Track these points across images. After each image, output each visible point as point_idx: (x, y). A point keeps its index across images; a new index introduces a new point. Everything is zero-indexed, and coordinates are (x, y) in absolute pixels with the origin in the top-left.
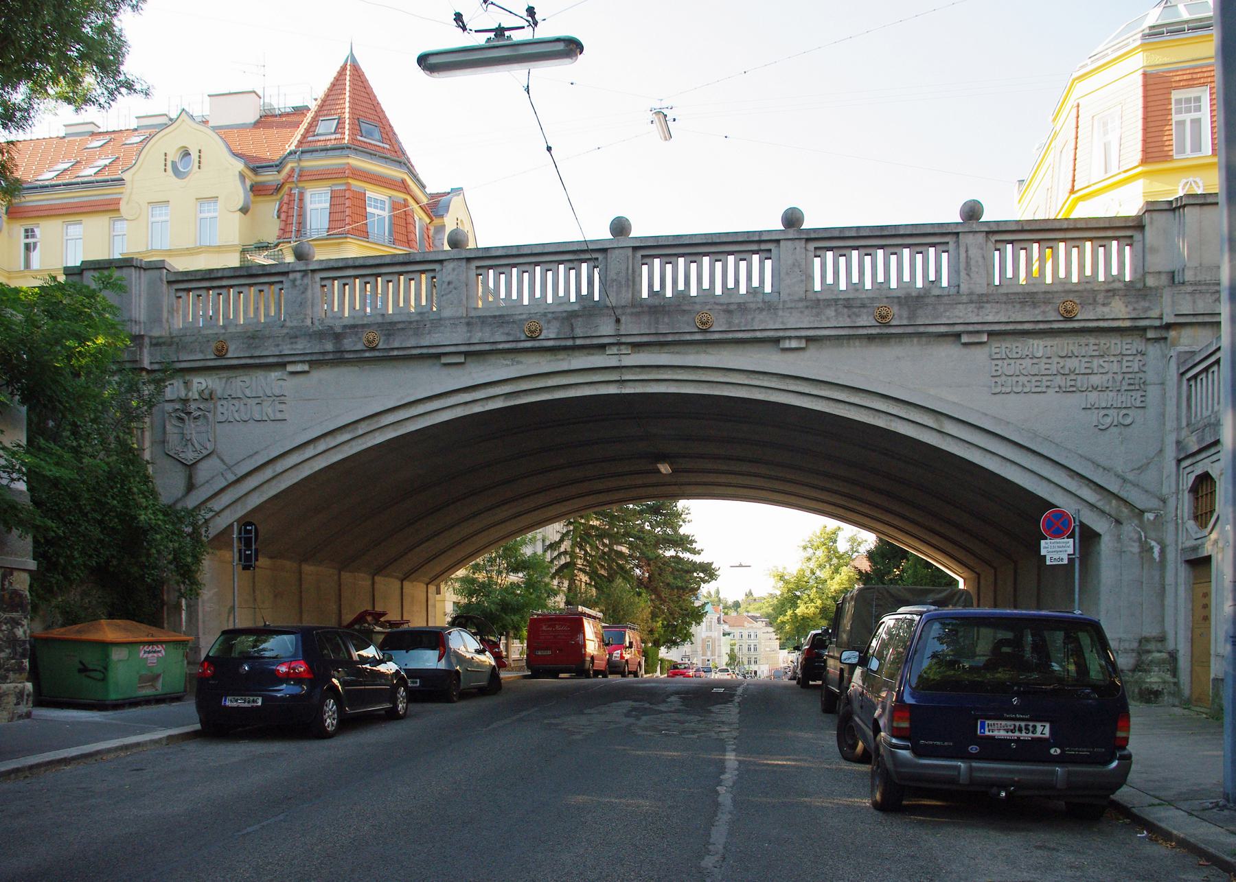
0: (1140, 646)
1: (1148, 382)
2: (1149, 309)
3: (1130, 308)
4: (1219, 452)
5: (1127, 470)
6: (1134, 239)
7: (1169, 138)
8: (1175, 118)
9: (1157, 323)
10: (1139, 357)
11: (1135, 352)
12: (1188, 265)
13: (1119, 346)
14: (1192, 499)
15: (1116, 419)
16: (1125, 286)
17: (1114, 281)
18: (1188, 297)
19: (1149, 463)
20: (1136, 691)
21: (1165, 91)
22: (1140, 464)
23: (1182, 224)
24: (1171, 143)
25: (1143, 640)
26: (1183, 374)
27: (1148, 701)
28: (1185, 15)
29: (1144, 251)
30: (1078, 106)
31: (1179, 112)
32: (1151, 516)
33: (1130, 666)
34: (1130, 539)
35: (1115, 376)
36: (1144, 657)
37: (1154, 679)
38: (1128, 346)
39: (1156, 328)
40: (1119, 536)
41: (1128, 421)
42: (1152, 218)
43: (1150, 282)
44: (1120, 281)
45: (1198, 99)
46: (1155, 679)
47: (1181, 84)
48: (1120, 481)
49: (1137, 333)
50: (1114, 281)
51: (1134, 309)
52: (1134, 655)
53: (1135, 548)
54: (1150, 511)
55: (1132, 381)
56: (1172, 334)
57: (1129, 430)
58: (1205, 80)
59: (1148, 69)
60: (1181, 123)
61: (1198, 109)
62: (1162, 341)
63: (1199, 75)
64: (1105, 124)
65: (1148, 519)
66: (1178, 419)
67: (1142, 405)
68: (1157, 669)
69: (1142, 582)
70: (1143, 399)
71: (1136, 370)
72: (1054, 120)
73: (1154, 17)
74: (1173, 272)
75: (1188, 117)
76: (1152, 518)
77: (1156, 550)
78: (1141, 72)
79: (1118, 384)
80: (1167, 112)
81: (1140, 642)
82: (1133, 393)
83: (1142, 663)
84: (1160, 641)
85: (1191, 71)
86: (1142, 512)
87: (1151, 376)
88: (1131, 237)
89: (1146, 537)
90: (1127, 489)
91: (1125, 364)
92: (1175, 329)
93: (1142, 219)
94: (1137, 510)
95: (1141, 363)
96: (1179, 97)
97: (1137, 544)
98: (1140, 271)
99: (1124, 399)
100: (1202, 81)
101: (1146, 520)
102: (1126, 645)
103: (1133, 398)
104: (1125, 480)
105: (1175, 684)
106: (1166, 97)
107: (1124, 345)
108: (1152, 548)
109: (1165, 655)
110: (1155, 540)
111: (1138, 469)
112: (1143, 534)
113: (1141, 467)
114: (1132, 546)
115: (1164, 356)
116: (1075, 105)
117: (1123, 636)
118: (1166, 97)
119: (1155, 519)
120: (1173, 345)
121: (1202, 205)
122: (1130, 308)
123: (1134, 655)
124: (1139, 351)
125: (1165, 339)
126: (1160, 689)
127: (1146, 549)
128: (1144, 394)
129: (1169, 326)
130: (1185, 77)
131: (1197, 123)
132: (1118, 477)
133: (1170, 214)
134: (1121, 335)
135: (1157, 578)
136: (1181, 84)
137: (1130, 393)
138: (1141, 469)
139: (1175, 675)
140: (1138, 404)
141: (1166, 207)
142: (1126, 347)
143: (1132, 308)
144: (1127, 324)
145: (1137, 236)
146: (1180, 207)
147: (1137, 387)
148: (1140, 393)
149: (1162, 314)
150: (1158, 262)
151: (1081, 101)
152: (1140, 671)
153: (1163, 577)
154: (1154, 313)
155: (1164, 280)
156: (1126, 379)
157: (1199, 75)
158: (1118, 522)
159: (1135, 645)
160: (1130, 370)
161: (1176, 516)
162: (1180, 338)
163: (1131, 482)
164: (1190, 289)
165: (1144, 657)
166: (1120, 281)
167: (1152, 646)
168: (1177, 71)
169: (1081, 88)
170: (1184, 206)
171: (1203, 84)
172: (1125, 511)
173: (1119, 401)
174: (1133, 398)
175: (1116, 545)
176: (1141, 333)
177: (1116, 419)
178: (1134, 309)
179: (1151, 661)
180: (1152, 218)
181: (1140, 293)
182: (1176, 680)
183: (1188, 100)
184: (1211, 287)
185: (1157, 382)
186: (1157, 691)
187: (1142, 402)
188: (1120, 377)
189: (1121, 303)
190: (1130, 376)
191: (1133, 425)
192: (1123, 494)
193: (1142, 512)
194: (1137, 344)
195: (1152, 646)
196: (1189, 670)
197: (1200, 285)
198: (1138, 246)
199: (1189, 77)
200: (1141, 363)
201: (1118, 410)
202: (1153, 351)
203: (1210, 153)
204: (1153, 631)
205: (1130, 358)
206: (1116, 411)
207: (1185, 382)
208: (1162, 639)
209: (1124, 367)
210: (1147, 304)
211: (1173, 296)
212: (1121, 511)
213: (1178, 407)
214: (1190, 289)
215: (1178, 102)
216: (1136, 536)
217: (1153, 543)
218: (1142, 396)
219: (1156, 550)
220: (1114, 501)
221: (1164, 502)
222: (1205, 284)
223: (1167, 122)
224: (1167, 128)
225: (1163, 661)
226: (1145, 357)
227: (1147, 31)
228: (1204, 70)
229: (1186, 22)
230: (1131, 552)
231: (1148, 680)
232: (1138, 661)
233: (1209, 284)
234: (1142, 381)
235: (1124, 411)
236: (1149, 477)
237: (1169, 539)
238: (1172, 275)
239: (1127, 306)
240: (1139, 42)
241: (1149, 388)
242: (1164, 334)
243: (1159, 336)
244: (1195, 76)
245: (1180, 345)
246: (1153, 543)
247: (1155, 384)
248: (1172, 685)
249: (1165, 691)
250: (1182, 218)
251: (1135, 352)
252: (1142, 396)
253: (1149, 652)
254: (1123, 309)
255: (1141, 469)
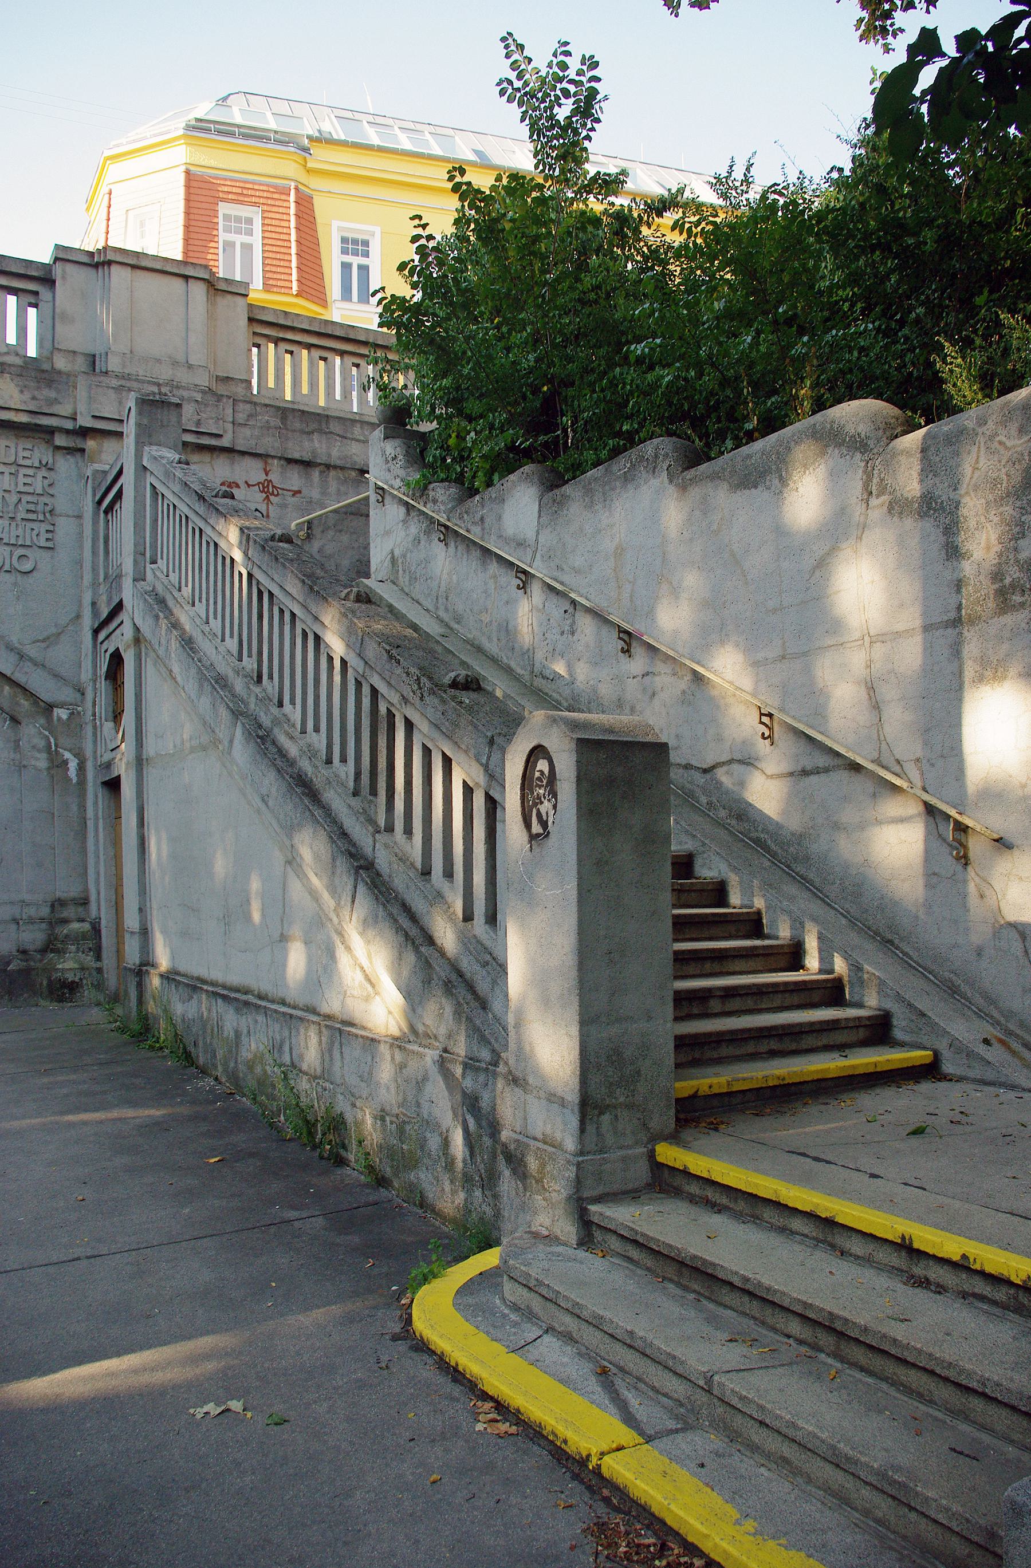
0: (53, 911)
1: (58, 511)
2: (56, 401)
3: (27, 396)
4: (122, 622)
5: (26, 642)
6: (41, 297)
7: (214, 257)
8: (223, 236)
9: (69, 425)
10: (44, 472)
11: (37, 464)
12: (113, 349)
13: (13, 450)
14: (110, 688)
15: (8, 562)
16: (25, 362)
17: (7, 353)
18: (111, 394)
19: (60, 634)
20: (45, 983)
21: (211, 200)
22: (45, 634)
23: (106, 289)
24: (216, 264)
25: (58, 904)
26: (100, 503)
27: (61, 999)
28: (239, 120)
29: (54, 318)
30: (110, 194)
31: (228, 230)
32: (63, 714)
33: (39, 944)
34: (34, 747)
35: (6, 495)
36: (58, 930)
37: (68, 965)
38: (27, 454)
39: (68, 432)
40: (17, 742)
41: (27, 566)
42: (64, 271)
43: (61, 363)
44: (17, 355)
45: (249, 221)
46: (70, 964)
47: (230, 196)
48: (13, 658)
49: (43, 436)
50: (7, 353)
51: (34, 398)
52: (44, 926)
53: (41, 762)
54: (61, 706)
55: (32, 507)
56: (91, 444)
57: (31, 579)
58: (257, 200)
59: (192, 168)
60: (229, 245)
61: (250, 233)
62: (78, 455)
63: (250, 192)
64: (142, 225)
65: (59, 719)
66: (94, 569)
67: (50, 544)
68: (73, 948)
69: (53, 814)
70: (50, 536)
71: (39, 491)
72: (88, 209)
73: (203, 110)
74: (94, 356)
75: (239, 239)
76: (65, 717)
77: (73, 765)
78: (183, 168)
79: (12, 507)
80: (211, 225)
81: (53, 906)
82: (34, 525)
83: (56, 939)
84: (81, 904)
85: (242, 185)
86: (50, 707)
87: (61, 504)
88: (36, 293)
89: (56, 746)
90: (25, 669)
91: (22, 480)
92: (94, 438)
93: (51, 271)
94: (42, 704)
95: (46, 482)
96: (227, 212)
97: (45, 755)
98: (48, 345)
99: (20, 532)
100: (254, 200)
101: (55, 718)
102: (32, 911)
103: (35, 532)
104: (22, 656)
105: (99, 970)
106: (212, 207)
107: (20, 449)
108: (66, 762)
109: (86, 926)
110: (70, 751)
111: (44, 641)
112: (52, 740)
113: (48, 638)
114: (37, 759)
115: (80, 476)
116: (107, 191)
117: (27, 897)
118: (212, 207)
119: (69, 718)
120: (92, 461)
121: (134, 267)
122: (27, 396)
123: (44, 926)
124: (44, 463)
125: (82, 451)
126: (77, 980)
127: (58, 765)
128: (51, 528)
129: (85, 432)
130: (234, 190)
131: (247, 248)
132: (12, 650)
133: (92, 272)
134: (17, 436)
135: (74, 808)
136: (230, 196)
137: (29, 525)
138: (49, 641)
139: (98, 957)
140: (43, 543)
141: (85, 259)
142: (22, 454)
143: (30, 396)
144: (24, 418)
145: (45, 293)
146: (103, 264)
147: (41, 517)
148: (44, 527)
149: (76, 413)
150: (72, 337)
151: (114, 188)
152: (53, 951)
153: (82, 807)
154: (65, 410)
155: (80, 364)
156: (24, 501)
157: (250, 192)
158: (15, 721)
159: (45, 911)
160: (31, 490)
161: (94, 715)
162: (101, 452)
163: (31, 660)
164: (115, 383)
165: (58, 930)
166: (17, 355)
167: (69, 912)
168: (226, 180)
169: (115, 171)
170: (110, 263)
171: (255, 204)
172: (25, 704)
173: (14, 533)
174: (35, 532)
175: (12, 755)
176: (47, 437)
177: (8, 562)
178: (34, 398)
179: (67, 936)
180: (64, 271)
181: (44, 376)
182: (98, 965)
183: (238, 220)
184: (145, 385)
185: (71, 513)
186: (73, 982)
187: (47, 539)
188: (13, 499)
189: (12, 385)
190: (30, 498)
191: (35, 573)
192: (20, 677)
193: (50, 707)
194: (41, 453)
195: (69, 912)
196: (114, 949)
197: (129, 379)
198: (45, 306)
199: (239, 191)
200: (46, 482)
201: (12, 548)
202: (65, 465)
203: (261, 288)
204: (73, 891)
205: (30, 472)
206: (8, 549)
207: (102, 515)
208: (84, 902)
209: (20, 484)
210: (53, 394)
211: (90, 387)
212: (17, 704)
213: (93, 552)
214: (115, 383)
215: (227, 218)
216: (42, 743)
217: (67, 755)
218: (47, 531)
219: (73, 765)
220: (7, 688)
221: (83, 694)
222: (137, 380)
223: (214, 238)
224: (212, 244)
225: (84, 936)
226: (52, 473)
227: (193, 123)
228: (256, 187)
229: (239, 126)
230: (35, 768)
231: (60, 966)
232: (49, 935)
233: (143, 382)
234: (48, 508)
235: (21, 551)
236: (60, 655)
237: (88, 753)
238: (92, 360)
239: (22, 392)
240: (181, 132)
241: (61, 522)
242: (79, 443)
243: (71, 444)
244: (245, 192)
245: (100, 462)
246: (67, 755)
247: (68, 516)
248: (94, 973)
249: (85, 982)
250: (107, 279)
251: (37, 464)
252: (47, 531)
253: (65, 921)
254: (16, 394)
255: (49, 641)
